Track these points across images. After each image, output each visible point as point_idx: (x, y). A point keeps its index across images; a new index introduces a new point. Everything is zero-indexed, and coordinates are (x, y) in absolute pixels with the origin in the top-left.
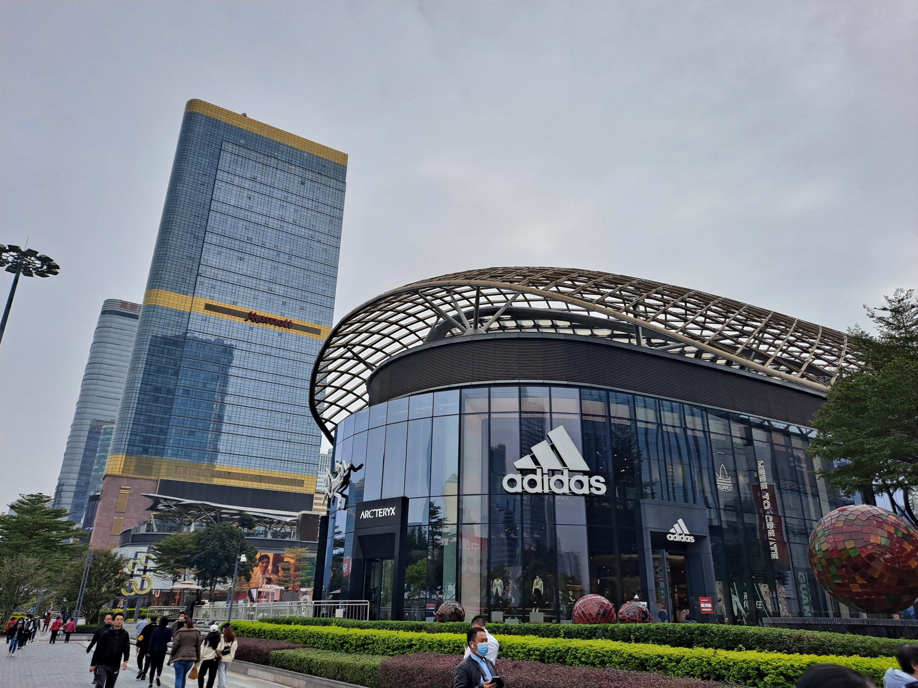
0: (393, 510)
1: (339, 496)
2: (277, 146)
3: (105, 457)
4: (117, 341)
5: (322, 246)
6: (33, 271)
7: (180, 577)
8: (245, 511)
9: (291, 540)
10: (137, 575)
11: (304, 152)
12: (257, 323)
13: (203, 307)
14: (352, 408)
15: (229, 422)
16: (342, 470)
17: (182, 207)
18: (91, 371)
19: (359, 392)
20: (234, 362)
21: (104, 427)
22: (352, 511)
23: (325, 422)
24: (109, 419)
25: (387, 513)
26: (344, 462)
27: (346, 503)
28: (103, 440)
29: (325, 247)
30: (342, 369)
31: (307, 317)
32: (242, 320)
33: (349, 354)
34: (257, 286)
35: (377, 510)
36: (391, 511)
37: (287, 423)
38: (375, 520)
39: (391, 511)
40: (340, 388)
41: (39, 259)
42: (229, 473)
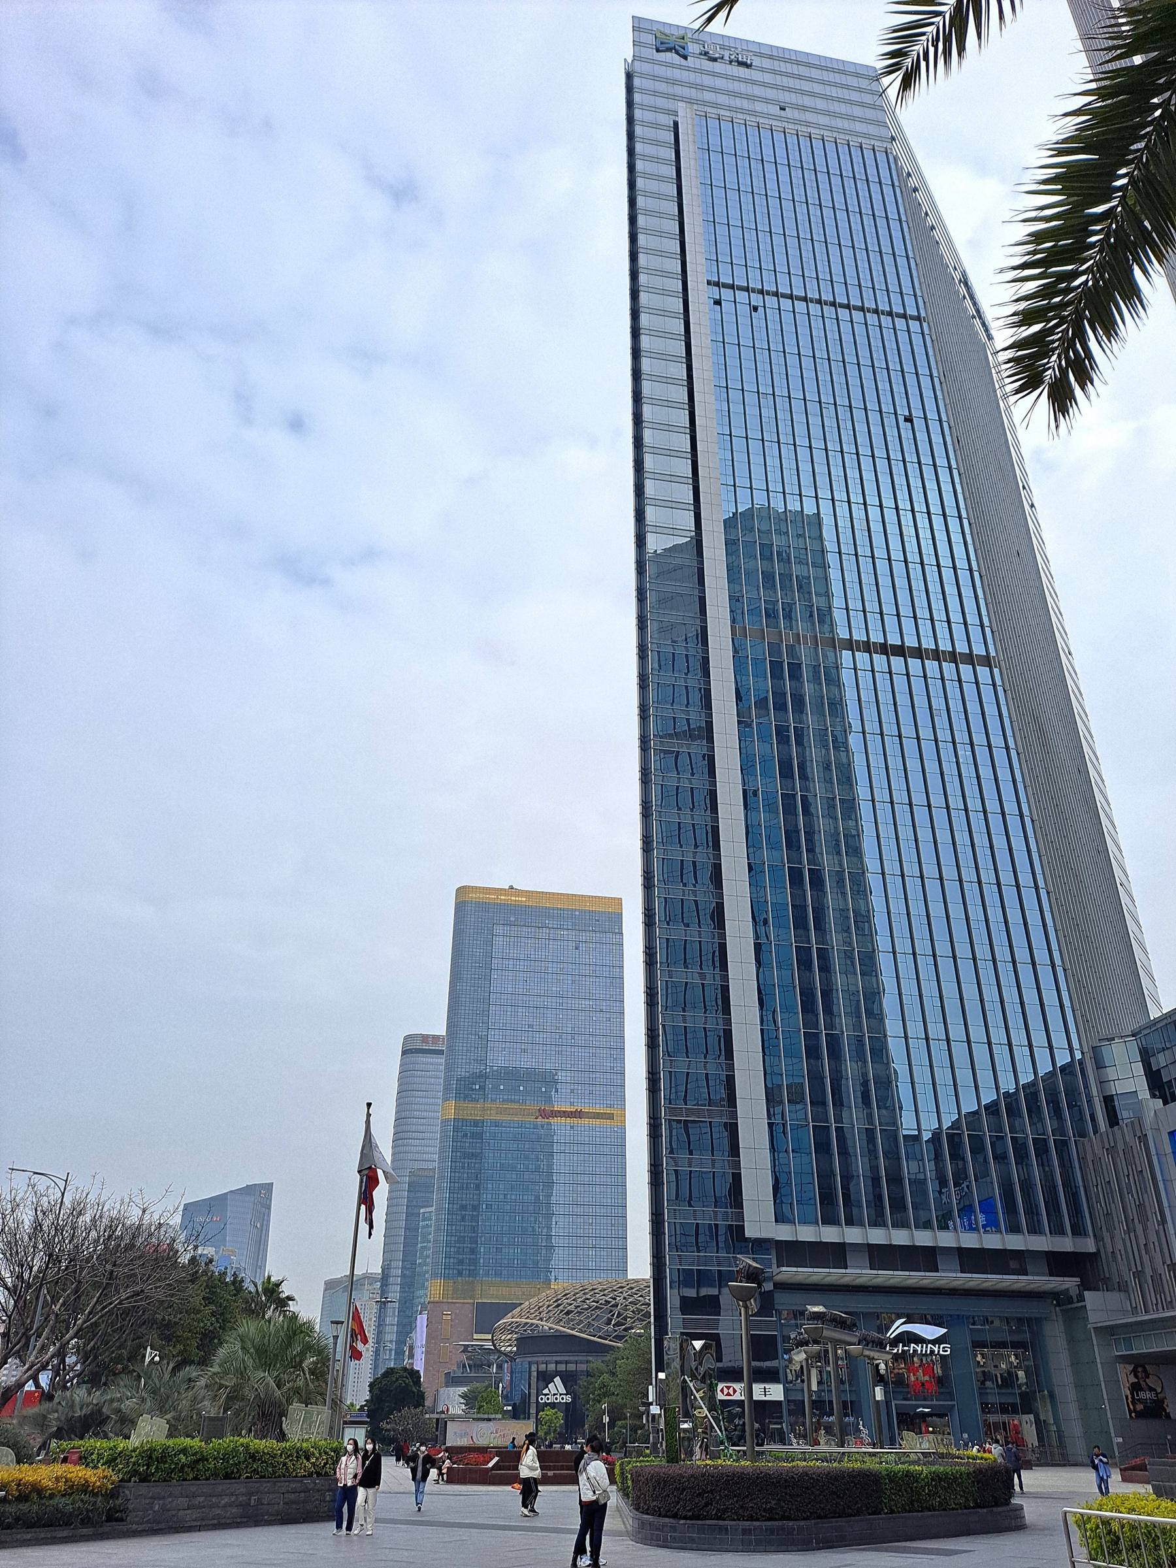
2: (547, 913)
4: (423, 1087)
17: (463, 1008)
18: (400, 1129)
21: (422, 1211)
28: (423, 1227)
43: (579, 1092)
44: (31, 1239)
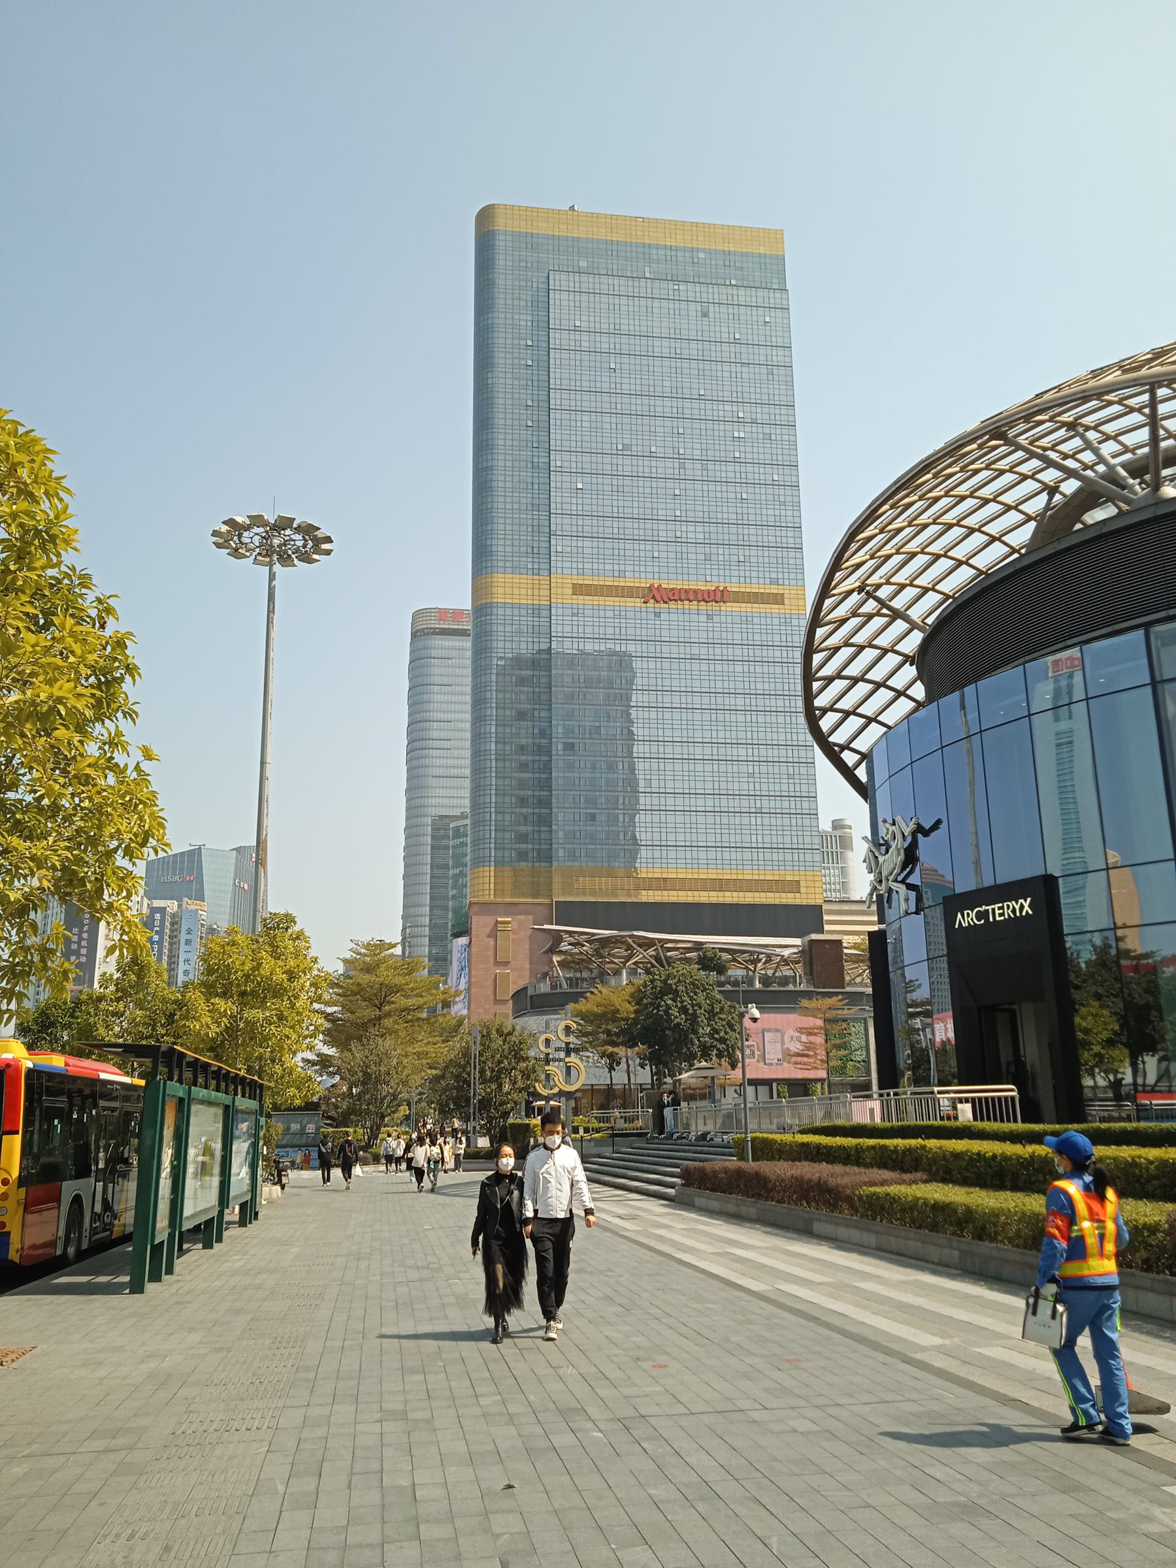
0: (1026, 905)
1: (902, 888)
3: (462, 874)
5: (760, 430)
6: (293, 556)
7: (619, 1064)
8: (706, 943)
9: (798, 989)
10: (555, 1060)
11: (698, 250)
12: (665, 602)
13: (570, 591)
14: (889, 717)
15: (648, 790)
16: (899, 837)
19: (898, 682)
20: (638, 681)
22: (938, 912)
23: (841, 752)
24: (457, 812)
25: (1014, 911)
26: (898, 819)
27: (919, 899)
28: (454, 847)
29: (767, 430)
30: (859, 639)
31: (754, 574)
32: (638, 602)
33: (871, 606)
34: (655, 533)
35: (990, 908)
36: (1022, 907)
37: (751, 780)
38: (990, 928)
39: (1025, 906)
40: (861, 679)
41: (298, 530)
42: (665, 879)
43: (721, 558)
44: (511, 1419)
